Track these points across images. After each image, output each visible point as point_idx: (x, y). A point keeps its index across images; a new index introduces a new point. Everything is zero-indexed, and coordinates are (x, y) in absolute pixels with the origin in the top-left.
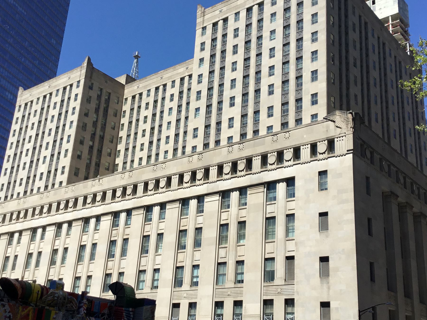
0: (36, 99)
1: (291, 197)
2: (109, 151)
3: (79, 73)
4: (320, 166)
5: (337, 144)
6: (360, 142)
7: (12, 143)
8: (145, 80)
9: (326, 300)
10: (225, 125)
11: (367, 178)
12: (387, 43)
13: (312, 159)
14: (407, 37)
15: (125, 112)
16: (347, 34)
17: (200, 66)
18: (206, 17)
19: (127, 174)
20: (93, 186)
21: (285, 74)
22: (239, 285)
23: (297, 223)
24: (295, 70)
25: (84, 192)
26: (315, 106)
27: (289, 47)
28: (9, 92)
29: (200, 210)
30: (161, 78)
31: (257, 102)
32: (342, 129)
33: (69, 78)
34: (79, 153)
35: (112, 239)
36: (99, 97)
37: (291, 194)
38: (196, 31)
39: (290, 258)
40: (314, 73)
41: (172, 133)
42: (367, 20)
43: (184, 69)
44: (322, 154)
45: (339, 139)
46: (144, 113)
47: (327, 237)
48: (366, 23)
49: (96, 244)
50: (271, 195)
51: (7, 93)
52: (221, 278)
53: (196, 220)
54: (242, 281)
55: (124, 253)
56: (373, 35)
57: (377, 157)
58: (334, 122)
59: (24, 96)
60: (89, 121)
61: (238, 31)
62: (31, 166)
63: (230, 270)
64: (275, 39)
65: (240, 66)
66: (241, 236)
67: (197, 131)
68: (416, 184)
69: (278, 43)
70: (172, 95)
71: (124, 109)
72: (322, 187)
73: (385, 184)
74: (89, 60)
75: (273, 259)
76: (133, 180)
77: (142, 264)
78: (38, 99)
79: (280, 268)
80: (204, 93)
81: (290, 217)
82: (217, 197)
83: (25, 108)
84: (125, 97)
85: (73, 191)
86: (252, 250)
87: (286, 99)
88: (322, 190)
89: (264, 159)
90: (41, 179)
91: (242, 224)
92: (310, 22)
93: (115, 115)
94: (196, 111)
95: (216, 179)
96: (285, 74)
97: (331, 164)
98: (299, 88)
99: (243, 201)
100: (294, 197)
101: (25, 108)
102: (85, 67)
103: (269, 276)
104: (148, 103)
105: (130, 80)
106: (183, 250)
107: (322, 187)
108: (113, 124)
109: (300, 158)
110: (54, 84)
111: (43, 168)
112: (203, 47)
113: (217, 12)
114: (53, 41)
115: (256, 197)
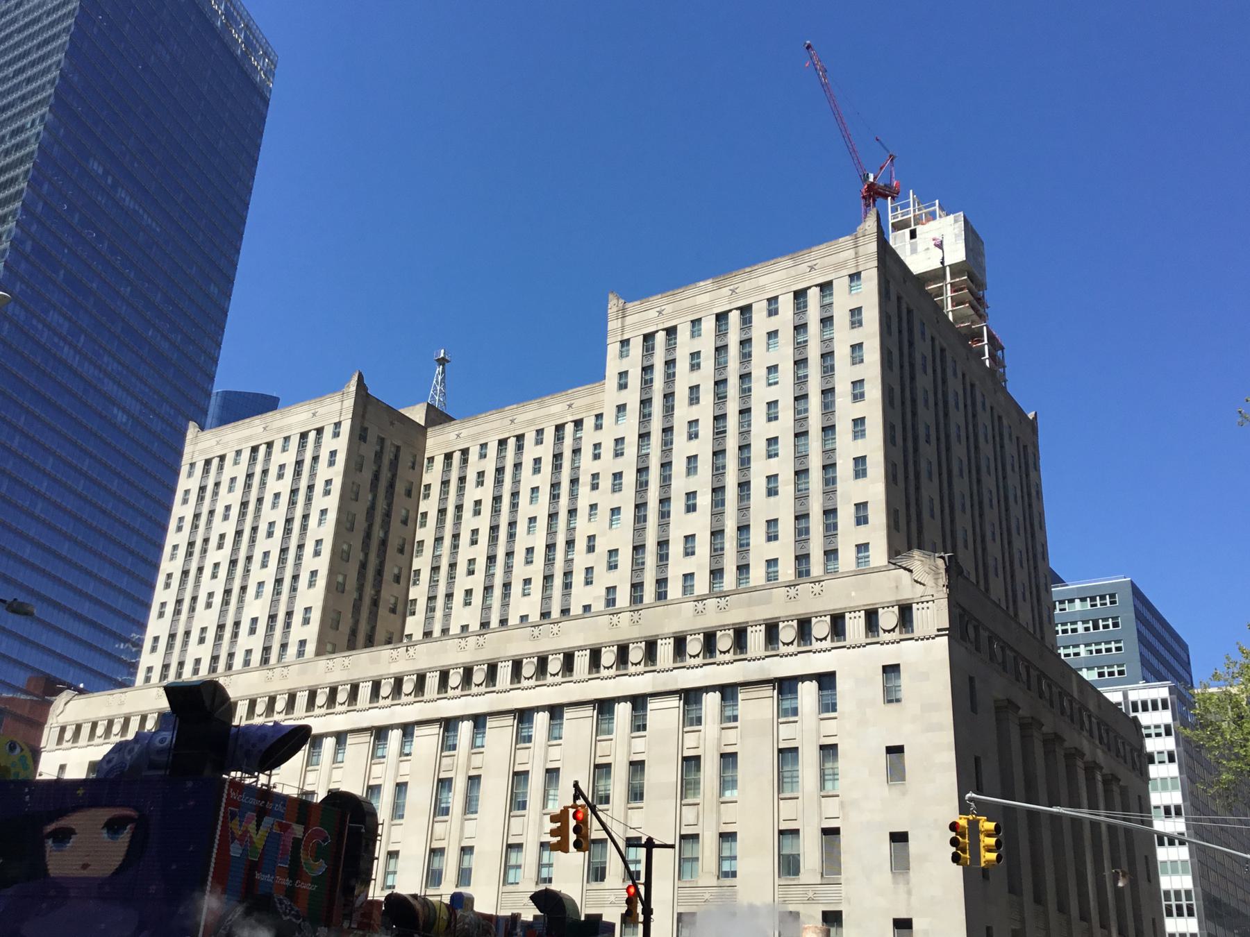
0: (234, 454)
1: (828, 711)
2: (396, 571)
3: (337, 406)
4: (888, 654)
5: (917, 614)
6: (958, 611)
7: (175, 547)
8: (473, 423)
9: (903, 915)
10: (676, 548)
11: (971, 679)
12: (977, 383)
13: (869, 641)
14: (982, 310)
15: (428, 487)
16: (913, 378)
17: (617, 421)
18: (629, 320)
19: (472, 640)
20: (394, 660)
21: (801, 456)
22: (728, 881)
23: (842, 763)
24: (820, 450)
25: (374, 672)
26: (862, 527)
27: (807, 403)
28: (119, 408)
29: (639, 725)
30: (512, 421)
31: (743, 509)
32: (924, 583)
33: (314, 414)
34: (340, 579)
35: (442, 775)
36: (379, 456)
37: (828, 706)
38: (606, 346)
39: (831, 833)
40: (860, 462)
41: (539, 541)
42: (945, 345)
43: (564, 406)
44: (889, 631)
45: (920, 605)
46: (472, 493)
47: (904, 794)
48: (942, 350)
49: (406, 784)
50: (787, 704)
51: (115, 411)
52: (687, 866)
53: (630, 745)
54: (734, 874)
55: (470, 806)
56: (955, 374)
57: (984, 634)
58: (910, 571)
59: (200, 444)
60: (360, 509)
61: (699, 357)
62: (226, 602)
63: (708, 847)
64: (776, 383)
65: (706, 429)
66: (727, 783)
67: (617, 555)
68: (1046, 677)
69: (784, 392)
70: (537, 461)
71: (425, 481)
72: (891, 696)
73: (997, 687)
74: (360, 378)
75: (796, 832)
76: (487, 654)
77: (513, 831)
78: (238, 453)
79: (810, 850)
80: (630, 479)
81: (829, 751)
82: (674, 702)
83: (206, 471)
84: (427, 455)
85: (345, 668)
86: (753, 809)
87: (803, 508)
88: (890, 701)
89: (772, 631)
90: (252, 631)
91: (729, 759)
92: (849, 360)
93: (409, 493)
94: (613, 515)
95: (670, 665)
96: (801, 456)
97: (905, 652)
98: (830, 487)
99: (729, 713)
100: (834, 710)
101: (206, 471)
102: (353, 395)
103: (789, 865)
104: (483, 472)
105: (437, 417)
106: (452, 753)
107: (891, 696)
108: (404, 512)
109: (844, 634)
110: (277, 424)
111: (257, 608)
112: (623, 381)
113: (653, 313)
114: (213, 289)
115: (757, 708)
